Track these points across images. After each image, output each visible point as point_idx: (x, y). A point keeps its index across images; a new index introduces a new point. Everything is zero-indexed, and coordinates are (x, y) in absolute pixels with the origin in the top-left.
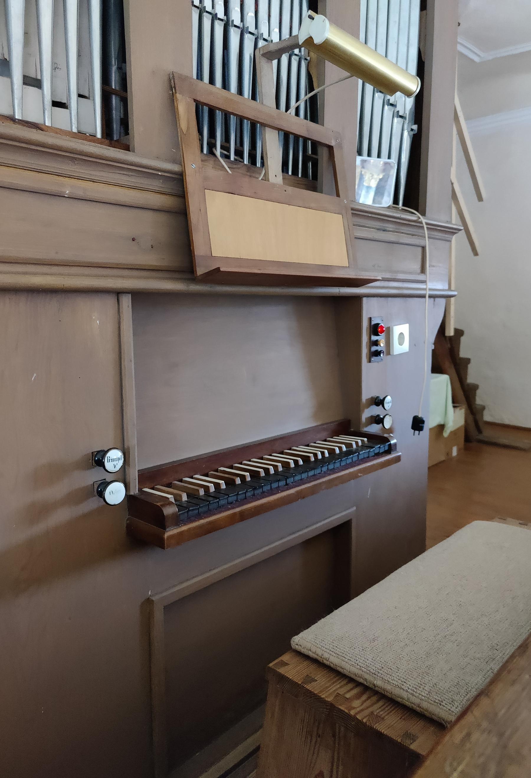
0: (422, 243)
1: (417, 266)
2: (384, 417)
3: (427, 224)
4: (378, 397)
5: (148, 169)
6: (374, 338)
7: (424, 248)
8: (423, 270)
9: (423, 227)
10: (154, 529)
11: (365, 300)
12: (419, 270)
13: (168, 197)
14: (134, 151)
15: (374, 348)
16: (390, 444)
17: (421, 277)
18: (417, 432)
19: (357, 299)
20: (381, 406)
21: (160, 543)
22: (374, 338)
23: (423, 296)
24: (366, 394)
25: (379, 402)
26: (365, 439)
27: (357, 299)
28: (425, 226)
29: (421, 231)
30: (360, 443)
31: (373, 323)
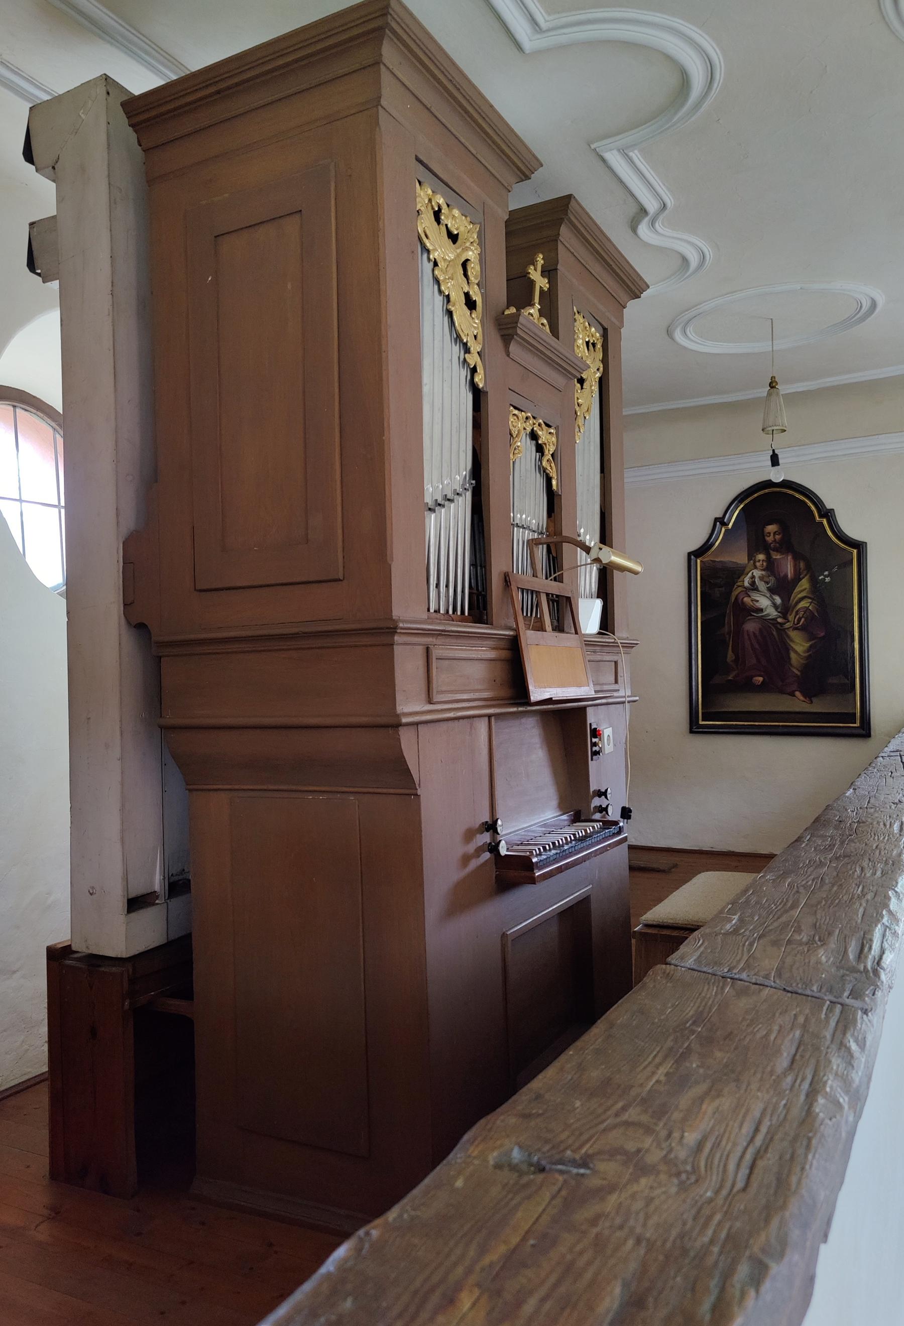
0: (615, 658)
1: (612, 679)
2: (607, 806)
3: (621, 643)
4: (599, 790)
5: (409, 633)
6: (594, 740)
7: (616, 663)
8: (616, 682)
9: (619, 646)
10: (527, 874)
11: (588, 709)
12: (613, 681)
13: (504, 651)
14: (492, 624)
15: (594, 749)
16: (620, 827)
17: (616, 687)
18: (626, 820)
19: (584, 709)
20: (603, 797)
21: (533, 881)
22: (594, 740)
23: (623, 703)
24: (593, 787)
25: (602, 794)
26: (601, 823)
27: (584, 709)
28: (620, 645)
29: (618, 649)
30: (599, 827)
31: (593, 727)
